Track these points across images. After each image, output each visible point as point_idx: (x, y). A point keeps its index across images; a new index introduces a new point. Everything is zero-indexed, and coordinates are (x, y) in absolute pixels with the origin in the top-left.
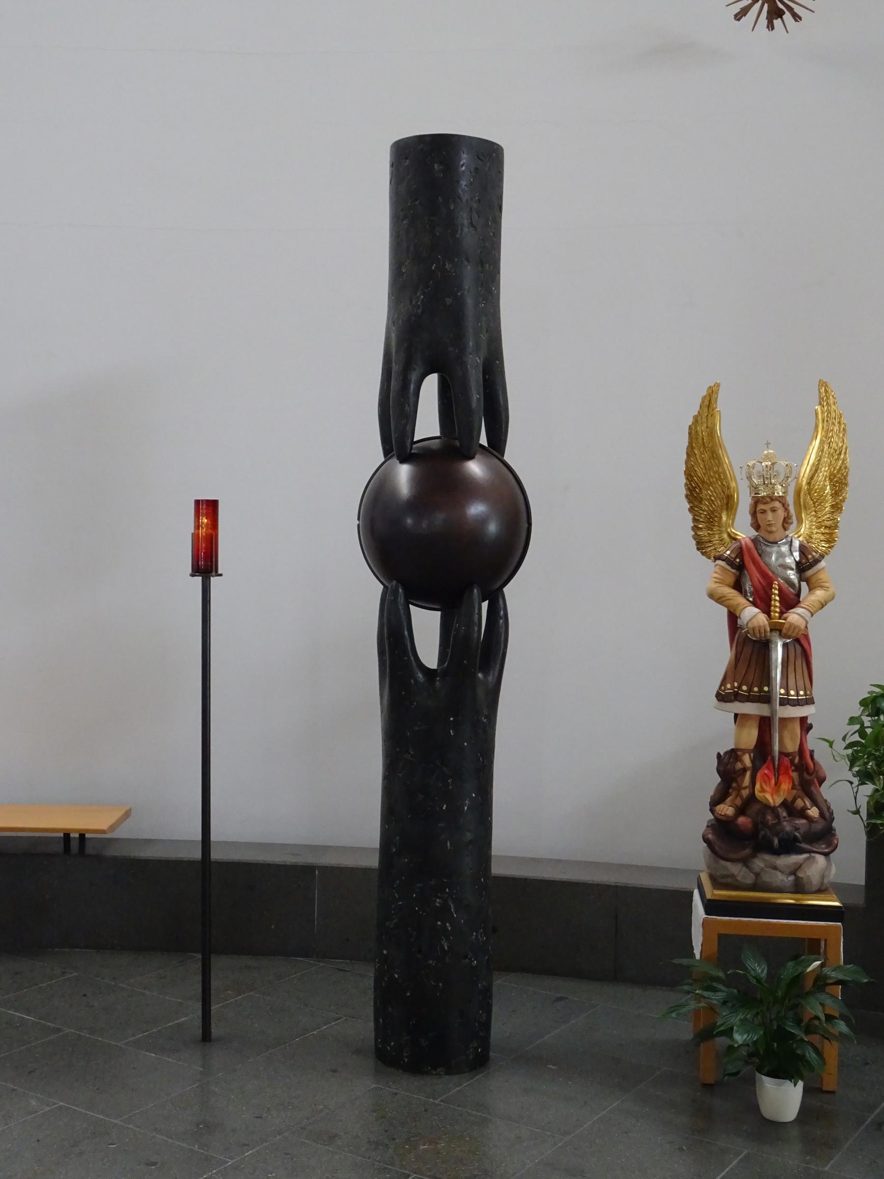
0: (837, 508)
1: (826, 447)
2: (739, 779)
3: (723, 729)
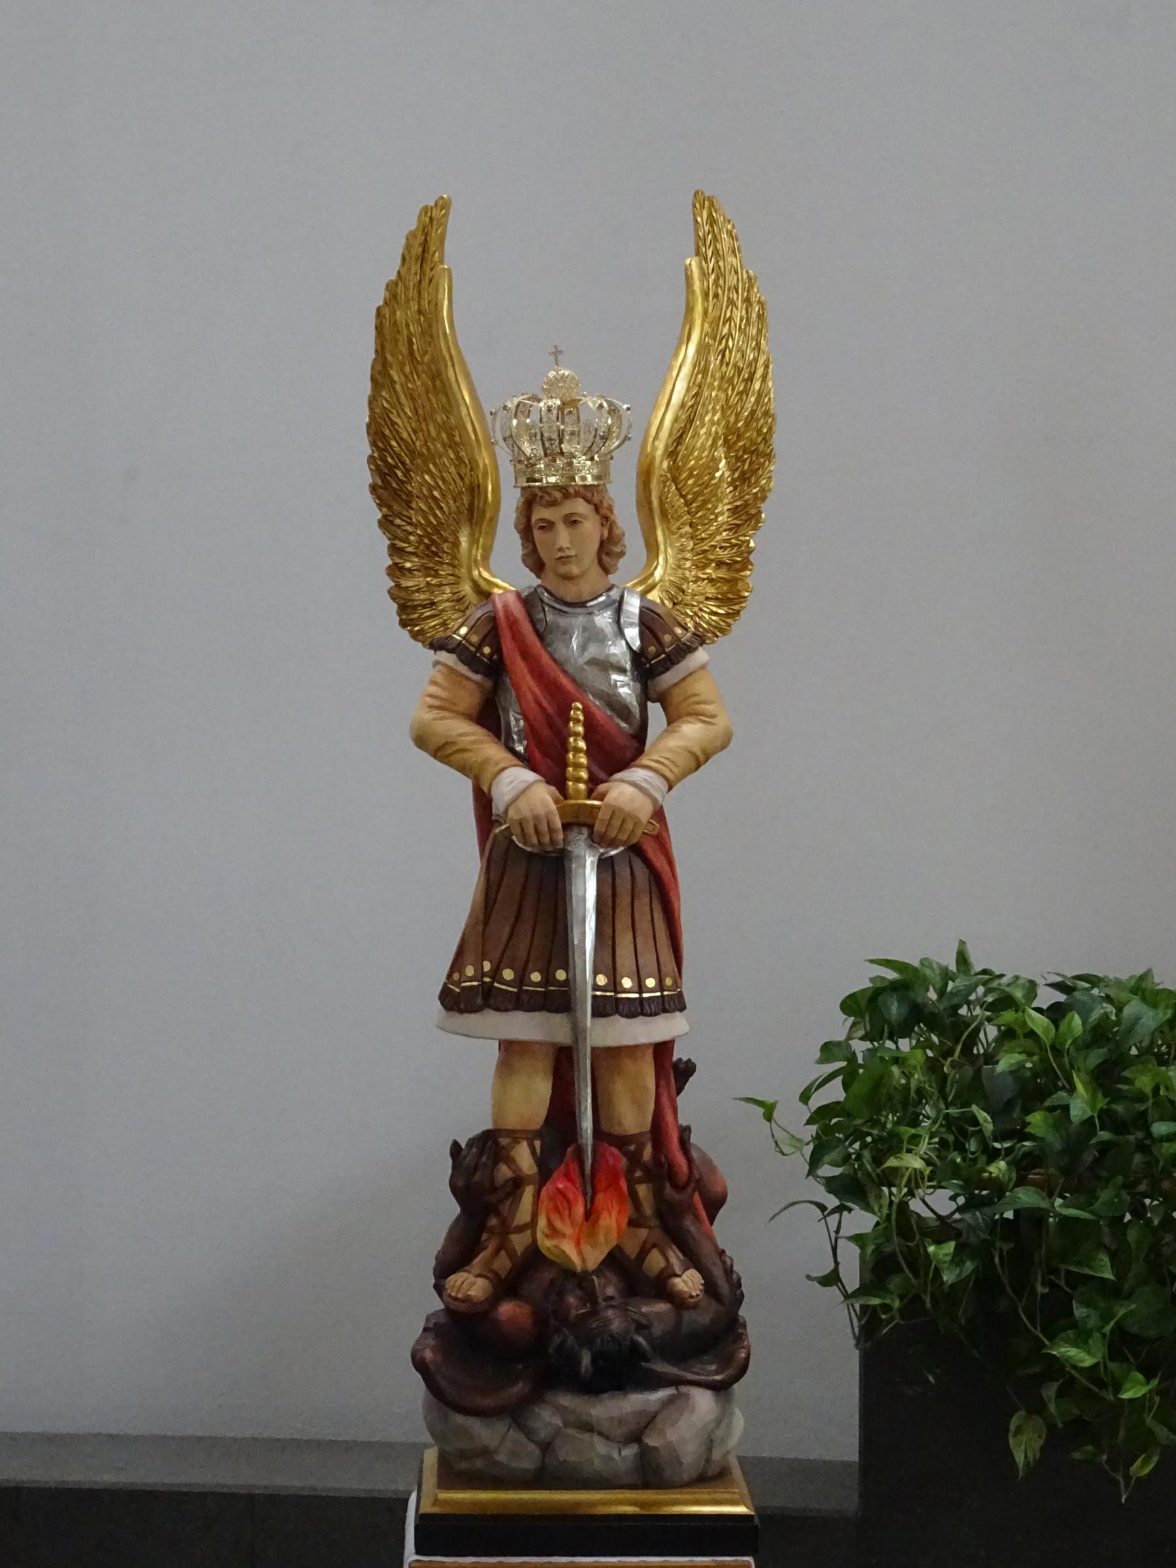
0: (746, 516)
1: (714, 362)
2: (505, 1208)
3: (466, 1080)
